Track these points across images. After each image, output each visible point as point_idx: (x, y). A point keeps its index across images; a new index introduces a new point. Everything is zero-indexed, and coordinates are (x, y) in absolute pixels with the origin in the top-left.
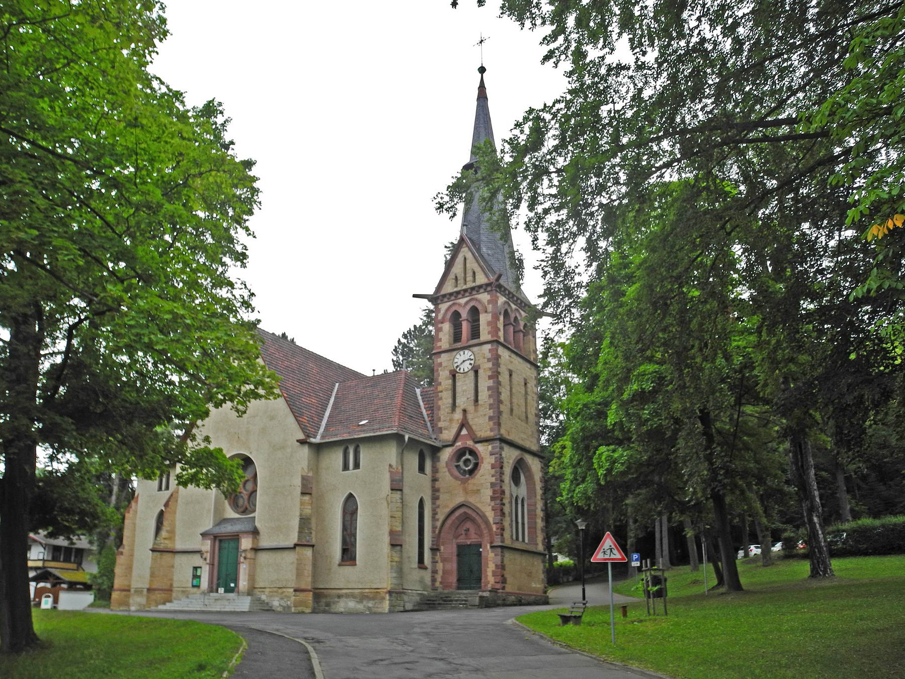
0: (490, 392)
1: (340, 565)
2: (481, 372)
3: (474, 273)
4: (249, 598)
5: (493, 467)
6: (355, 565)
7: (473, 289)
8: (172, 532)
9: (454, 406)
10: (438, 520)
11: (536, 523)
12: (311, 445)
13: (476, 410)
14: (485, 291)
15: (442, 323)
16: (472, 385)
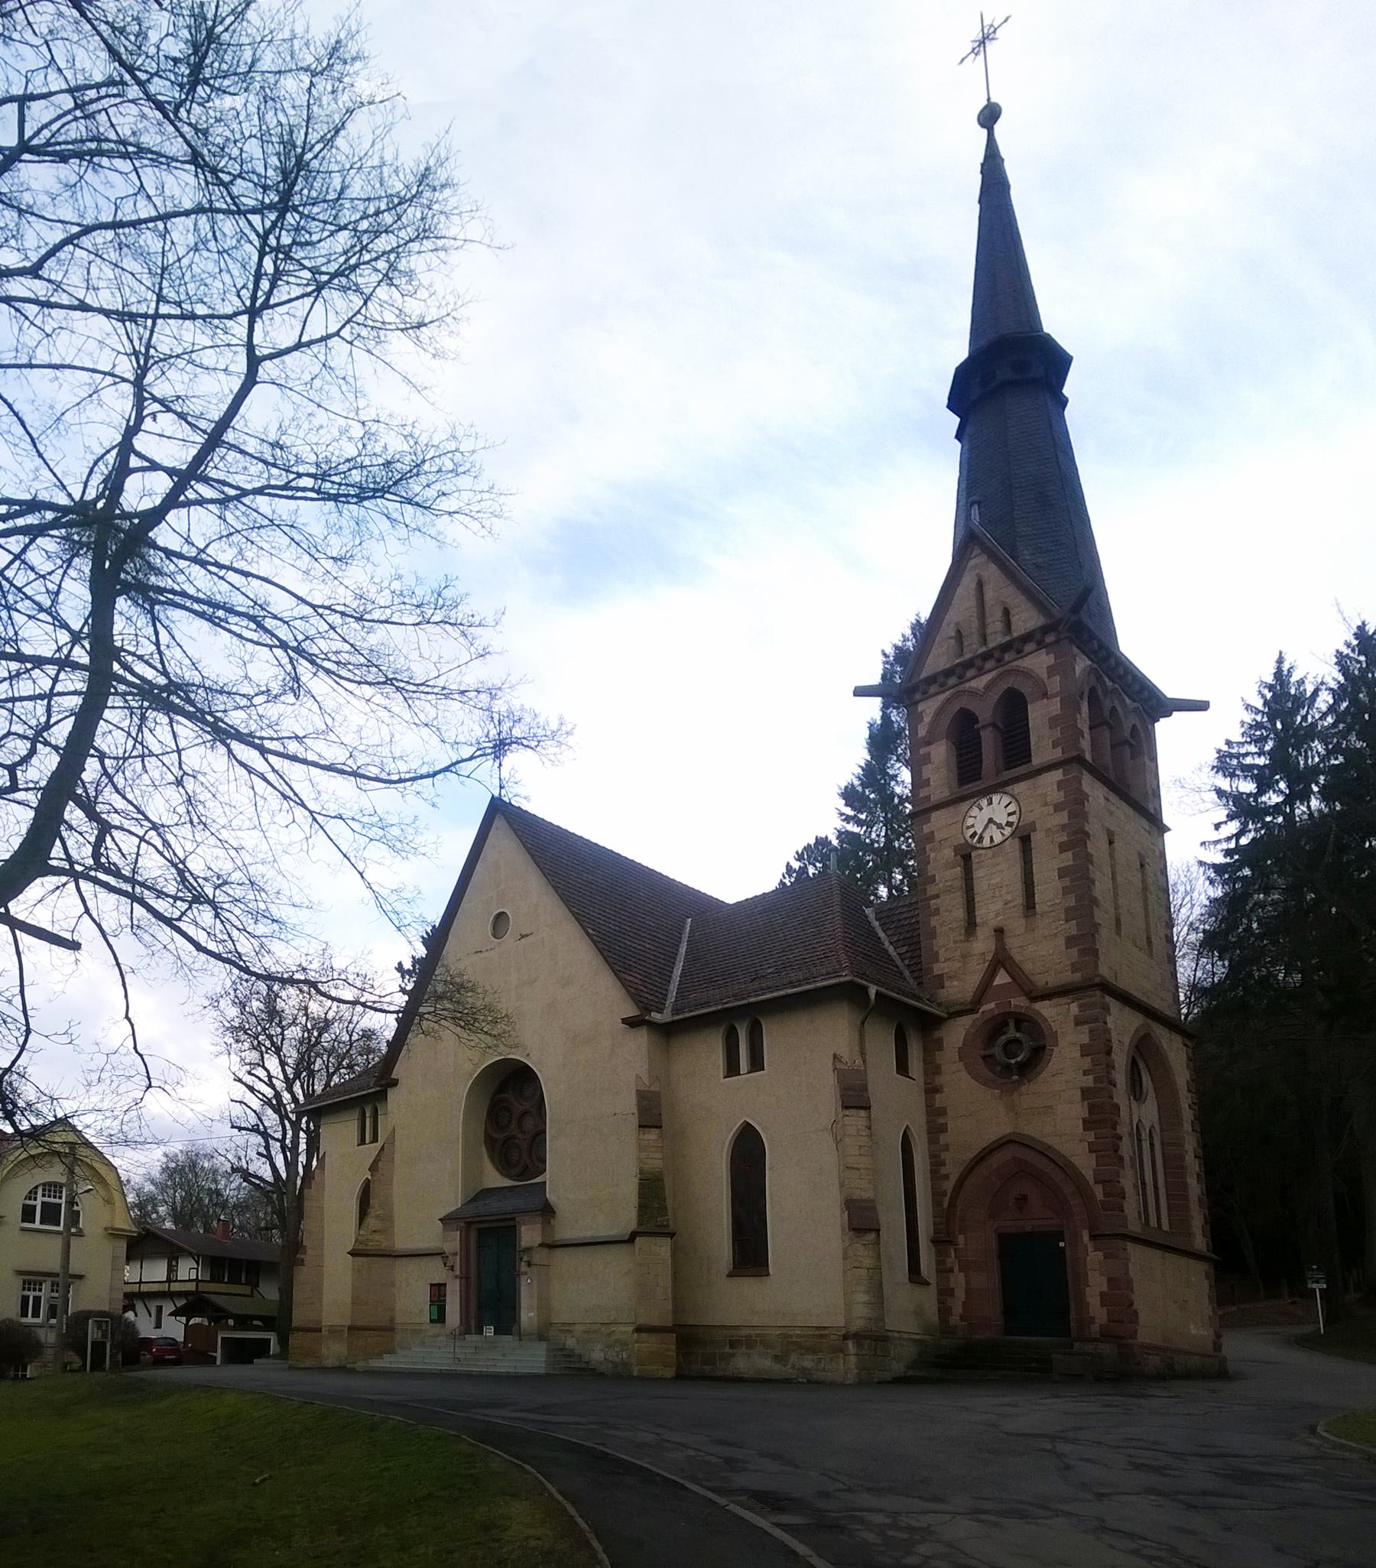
0: (1067, 881)
1: (730, 1275)
2: (1037, 838)
3: (1006, 613)
4: (544, 1345)
5: (1085, 1051)
6: (768, 1274)
7: (1005, 648)
8: (388, 1218)
9: (971, 925)
10: (946, 1177)
11: (1185, 1185)
12: (652, 1026)
13: (1030, 929)
14: (1041, 645)
15: (929, 743)
16: (1017, 870)
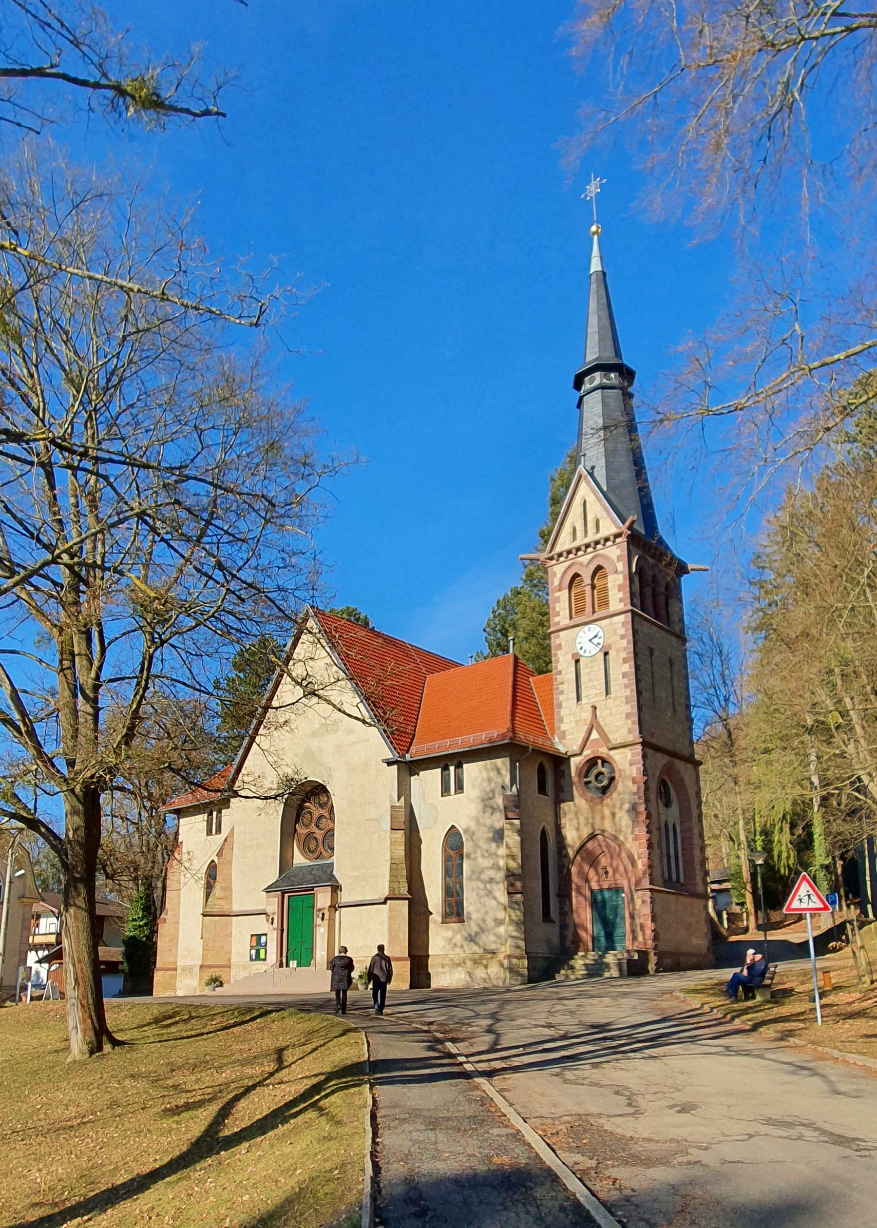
0: (625, 681)
8: (228, 889)
